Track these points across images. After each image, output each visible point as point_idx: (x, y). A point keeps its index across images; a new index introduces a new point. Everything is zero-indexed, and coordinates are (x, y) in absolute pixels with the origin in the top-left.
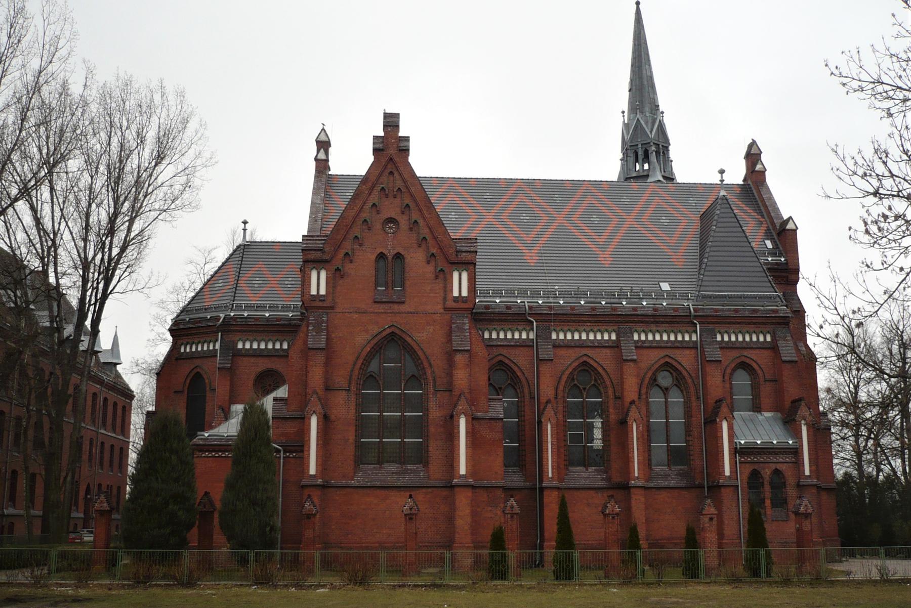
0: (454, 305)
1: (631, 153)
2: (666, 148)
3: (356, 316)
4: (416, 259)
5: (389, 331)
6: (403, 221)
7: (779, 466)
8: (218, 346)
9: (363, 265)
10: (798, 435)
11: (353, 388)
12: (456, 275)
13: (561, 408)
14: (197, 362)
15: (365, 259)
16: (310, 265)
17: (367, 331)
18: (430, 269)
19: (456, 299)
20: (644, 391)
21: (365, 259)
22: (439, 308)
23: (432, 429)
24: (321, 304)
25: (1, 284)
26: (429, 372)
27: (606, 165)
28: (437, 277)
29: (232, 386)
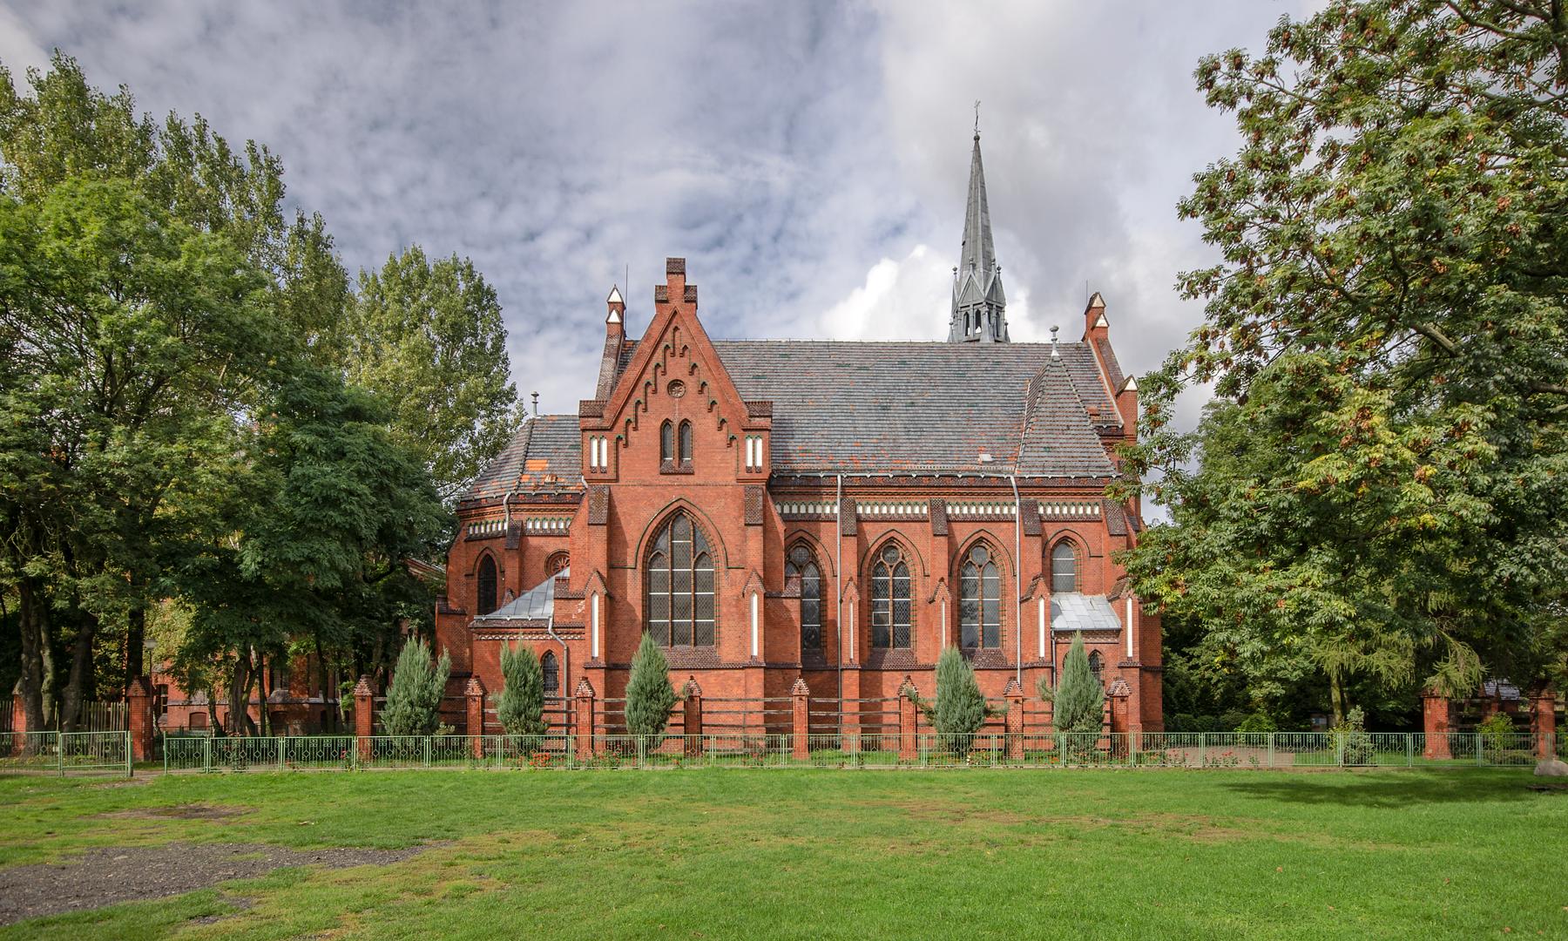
0: (748, 476)
1: (962, 316)
2: (1000, 309)
3: (641, 489)
4: (704, 426)
5: (676, 505)
6: (691, 384)
7: (1098, 647)
8: (836, 510)
9: (646, 436)
10: (1122, 615)
11: (639, 567)
12: (750, 442)
13: (865, 586)
14: (486, 543)
15: (650, 425)
16: (590, 434)
17: (652, 505)
18: (721, 437)
19: (749, 470)
20: (955, 567)
21: (650, 425)
22: (732, 480)
23: (724, 610)
24: (601, 476)
25: (1086, 940)
26: (720, 548)
27: (939, 327)
28: (730, 445)
29: (522, 568)
